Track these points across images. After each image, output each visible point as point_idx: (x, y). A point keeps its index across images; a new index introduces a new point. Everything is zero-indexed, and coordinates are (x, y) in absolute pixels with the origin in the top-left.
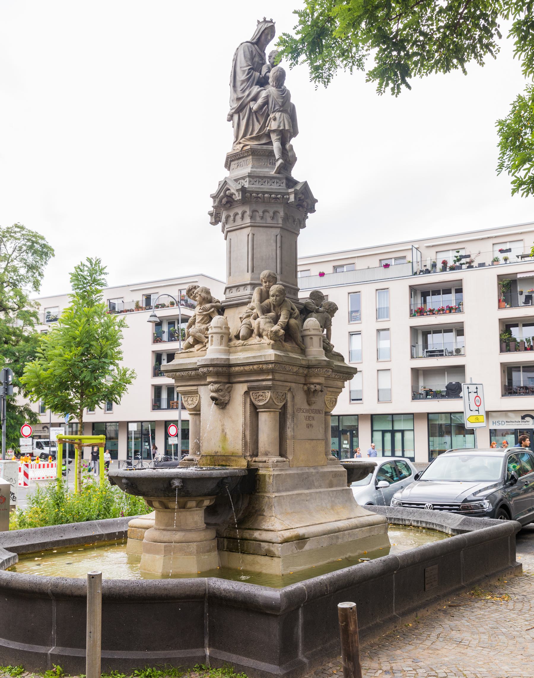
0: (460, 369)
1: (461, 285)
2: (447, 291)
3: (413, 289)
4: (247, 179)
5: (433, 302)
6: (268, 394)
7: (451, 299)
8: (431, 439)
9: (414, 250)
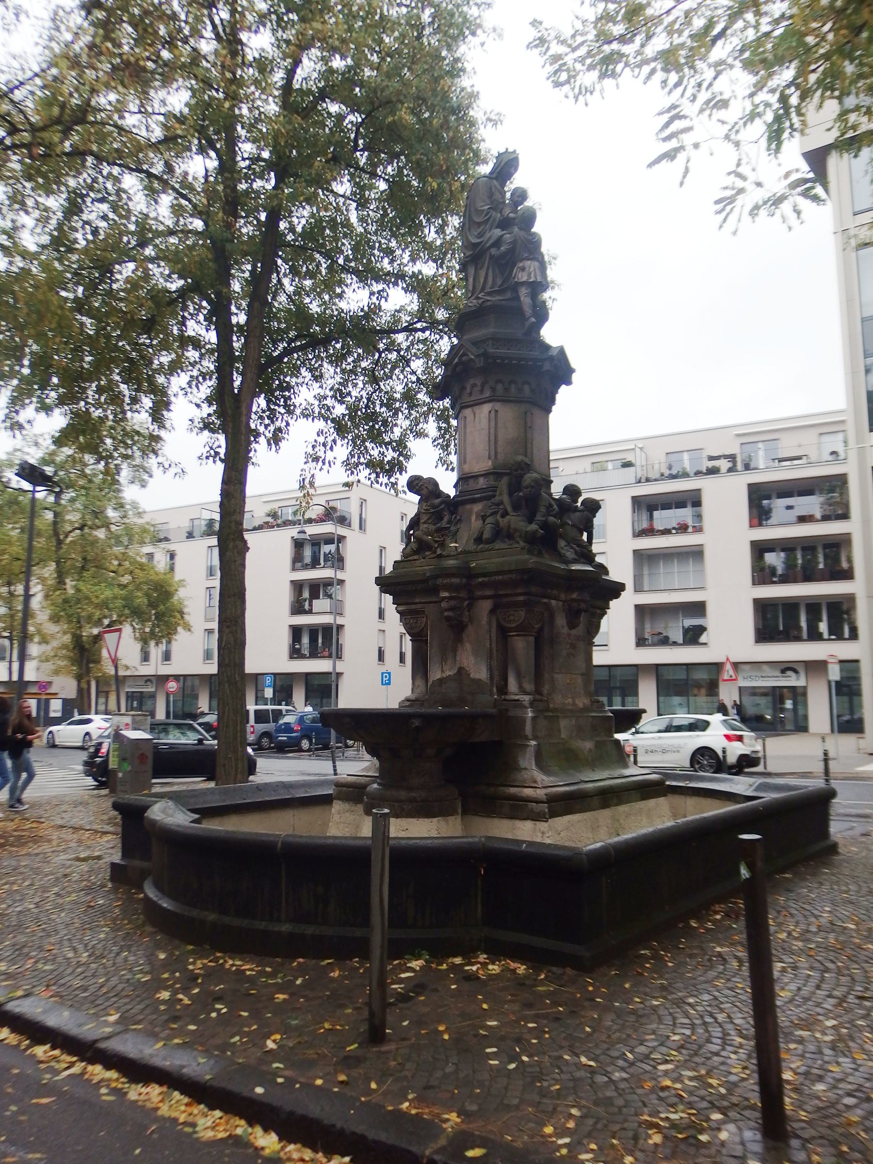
0: (698, 609)
1: (699, 496)
2: (681, 505)
3: (637, 502)
4: (490, 342)
5: (663, 518)
6: (522, 614)
7: (685, 514)
8: (661, 699)
9: (638, 450)
